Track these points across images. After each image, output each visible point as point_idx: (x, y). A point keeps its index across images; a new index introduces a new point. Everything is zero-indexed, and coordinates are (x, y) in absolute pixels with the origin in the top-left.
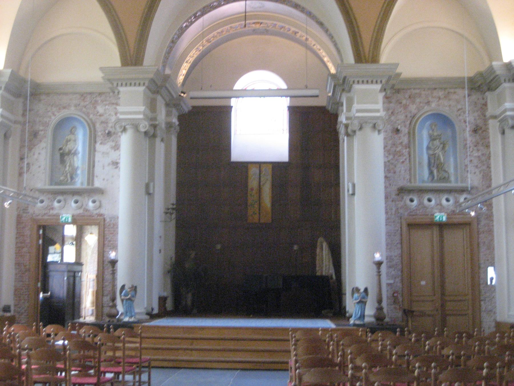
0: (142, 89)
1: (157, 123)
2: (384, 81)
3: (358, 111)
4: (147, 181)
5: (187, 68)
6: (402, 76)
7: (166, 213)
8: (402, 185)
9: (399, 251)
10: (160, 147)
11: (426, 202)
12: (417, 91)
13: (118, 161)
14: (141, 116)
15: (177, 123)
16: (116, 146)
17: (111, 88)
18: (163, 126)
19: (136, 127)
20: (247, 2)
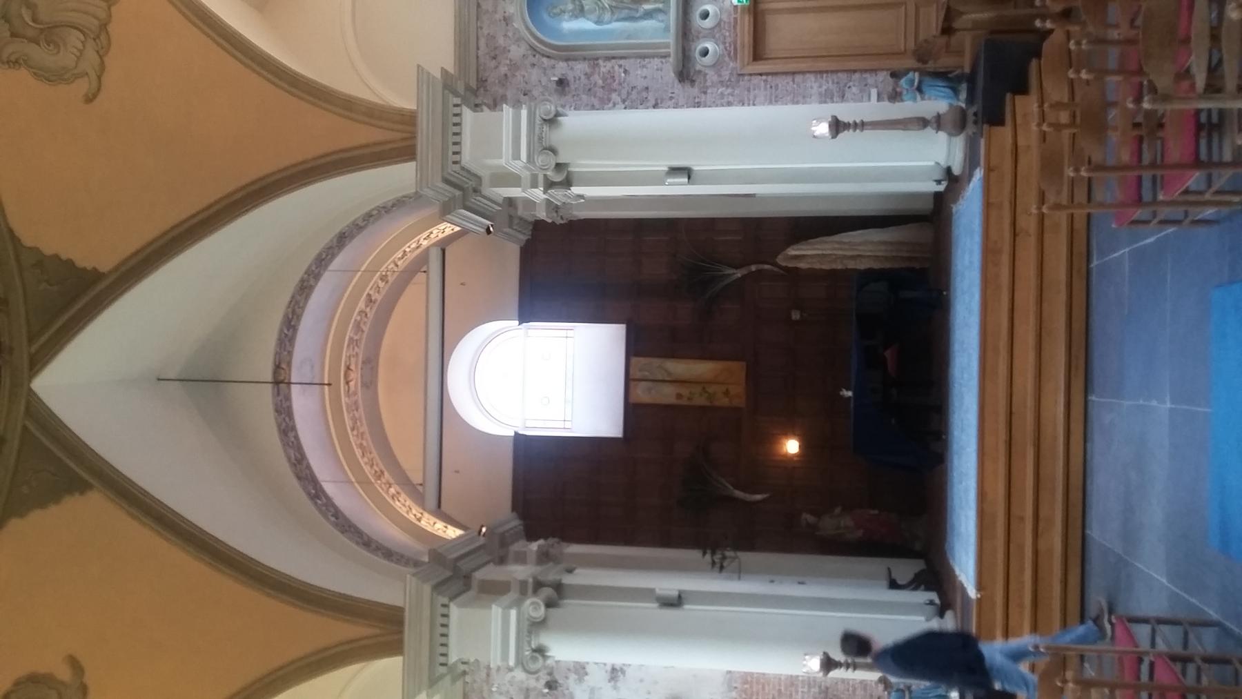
0: (454, 611)
1: (531, 580)
2: (457, 101)
3: (516, 156)
4: (656, 605)
5: (433, 519)
6: (451, 68)
7: (722, 568)
8: (672, 75)
9: (811, 77)
10: (583, 577)
11: (708, 24)
12: (482, 42)
13: (609, 668)
14: (513, 613)
15: (541, 542)
16: (576, 672)
17: (454, 681)
18: (539, 568)
19: (538, 625)
20: (293, 380)
